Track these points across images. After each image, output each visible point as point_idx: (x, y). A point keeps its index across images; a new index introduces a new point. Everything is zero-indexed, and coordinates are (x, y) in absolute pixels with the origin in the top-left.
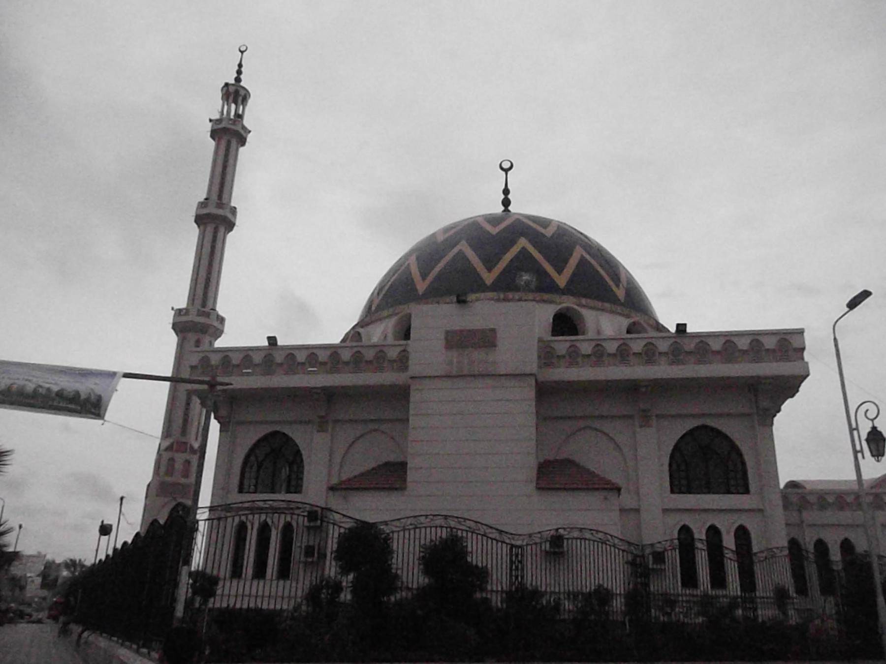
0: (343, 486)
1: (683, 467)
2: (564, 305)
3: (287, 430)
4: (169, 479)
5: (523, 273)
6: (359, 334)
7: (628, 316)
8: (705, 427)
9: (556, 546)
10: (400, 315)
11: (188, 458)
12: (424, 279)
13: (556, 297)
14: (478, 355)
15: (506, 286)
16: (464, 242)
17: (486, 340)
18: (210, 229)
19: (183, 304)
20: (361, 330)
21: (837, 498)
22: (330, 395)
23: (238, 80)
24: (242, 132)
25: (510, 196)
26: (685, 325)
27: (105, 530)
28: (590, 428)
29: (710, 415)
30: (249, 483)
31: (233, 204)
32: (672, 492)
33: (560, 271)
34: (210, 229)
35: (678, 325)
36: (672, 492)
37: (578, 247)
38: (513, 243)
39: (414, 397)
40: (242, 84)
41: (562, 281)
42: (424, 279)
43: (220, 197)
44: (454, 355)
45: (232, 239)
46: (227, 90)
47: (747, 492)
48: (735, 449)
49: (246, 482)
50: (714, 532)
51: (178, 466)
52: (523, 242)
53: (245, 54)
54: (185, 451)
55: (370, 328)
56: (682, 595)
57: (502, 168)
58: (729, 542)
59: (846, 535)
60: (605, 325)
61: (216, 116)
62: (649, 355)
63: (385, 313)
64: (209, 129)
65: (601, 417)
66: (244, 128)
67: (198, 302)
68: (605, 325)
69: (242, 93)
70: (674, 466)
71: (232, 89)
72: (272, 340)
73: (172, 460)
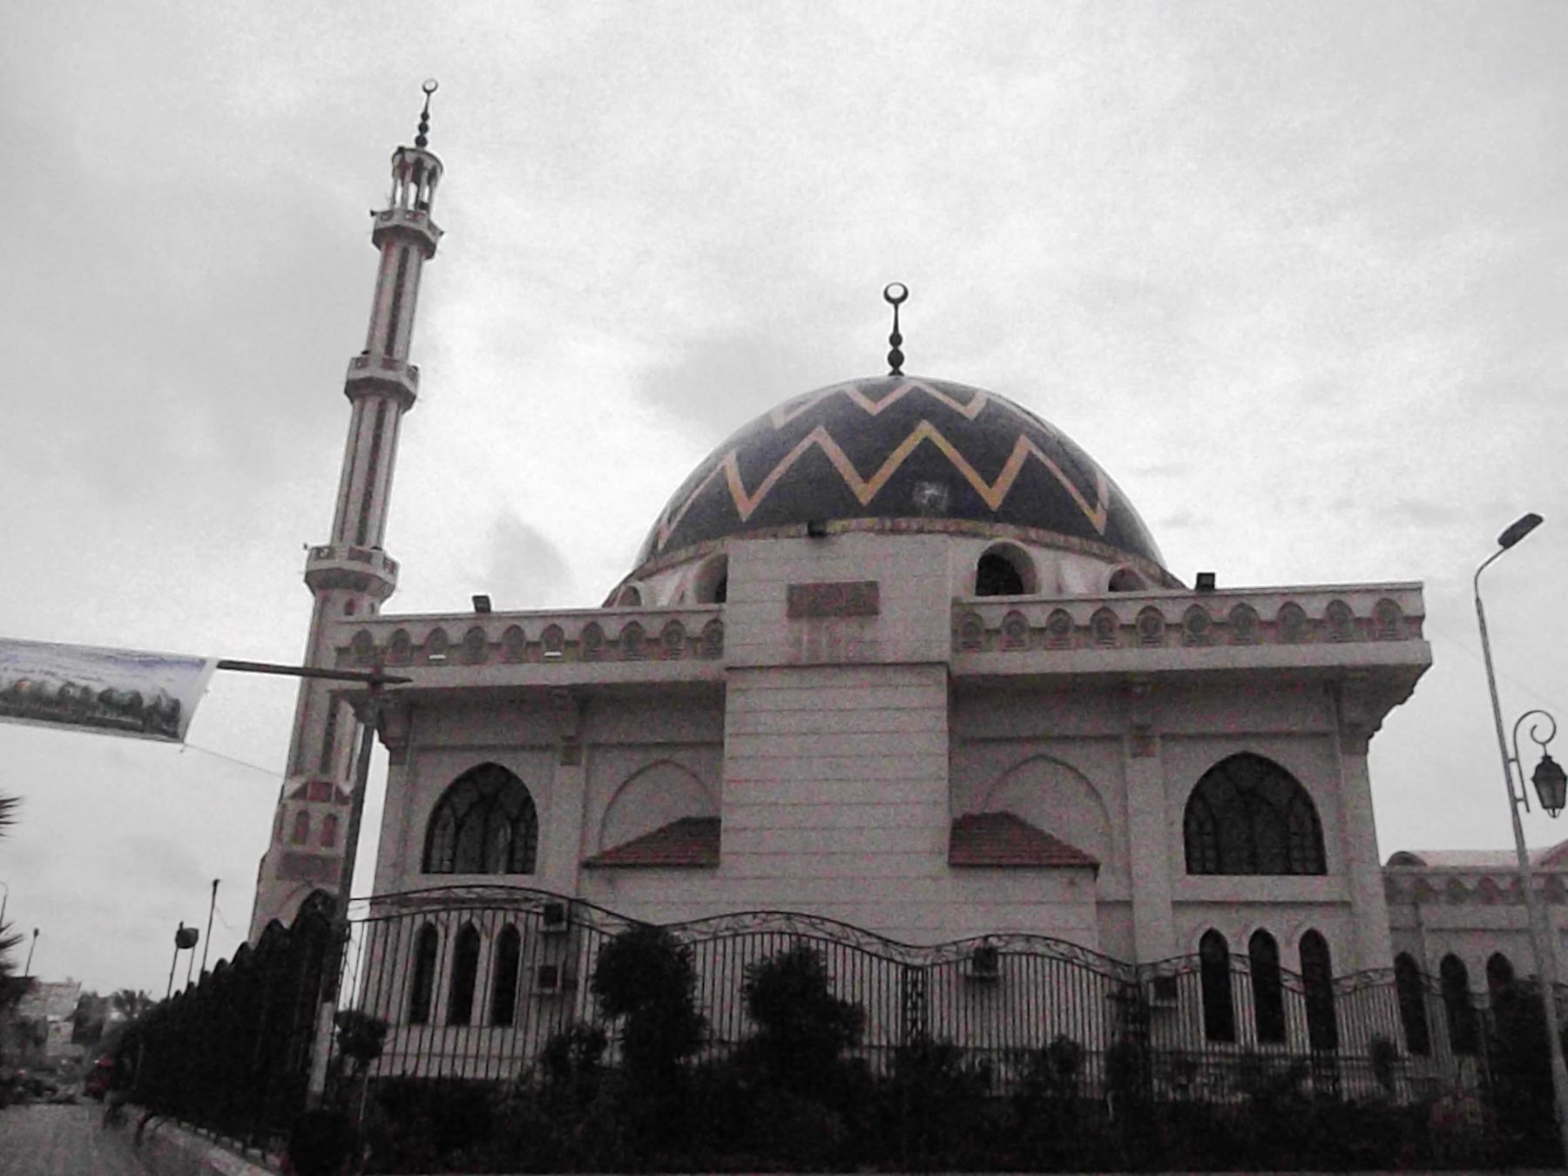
1: (1209, 828)
2: (999, 540)
3: (507, 762)
4: (298, 848)
5: (926, 484)
6: (635, 591)
7: (1111, 560)
8: (1247, 756)
9: (984, 968)
10: (707, 558)
11: (333, 811)
12: (750, 494)
13: (985, 528)
14: (846, 629)
15: (896, 506)
16: (821, 429)
17: (860, 601)
18: (371, 406)
19: (323, 538)
20: (639, 585)
21: (1481, 883)
22: (584, 699)
23: (421, 141)
24: (429, 234)
25: (902, 348)
26: (1212, 575)
27: (186, 939)
28: (1043, 757)
29: (1257, 736)
30: (440, 855)
31: (412, 362)
32: (1190, 871)
33: (990, 481)
34: (371, 406)
35: (1200, 576)
36: (1190, 871)
37: (1023, 438)
38: (908, 429)
39: (733, 703)
40: (428, 148)
41: (994, 497)
42: (750, 494)
43: (389, 348)
44: (804, 627)
46: (403, 160)
47: (1321, 870)
48: (1300, 795)
49: (436, 855)
50: (1263, 942)
51: (316, 825)
52: (925, 429)
53: (433, 95)
54: (328, 799)
55: (656, 581)
56: (1207, 1055)
57: (888, 298)
58: (1290, 959)
60: (1069, 574)
61: (383, 206)
62: (1149, 628)
63: (682, 554)
64: (371, 229)
65: (1065, 739)
66: (431, 226)
68: (1069, 574)
69: (429, 164)
70: (1194, 826)
71: (410, 158)
72: (482, 603)
73: (304, 815)
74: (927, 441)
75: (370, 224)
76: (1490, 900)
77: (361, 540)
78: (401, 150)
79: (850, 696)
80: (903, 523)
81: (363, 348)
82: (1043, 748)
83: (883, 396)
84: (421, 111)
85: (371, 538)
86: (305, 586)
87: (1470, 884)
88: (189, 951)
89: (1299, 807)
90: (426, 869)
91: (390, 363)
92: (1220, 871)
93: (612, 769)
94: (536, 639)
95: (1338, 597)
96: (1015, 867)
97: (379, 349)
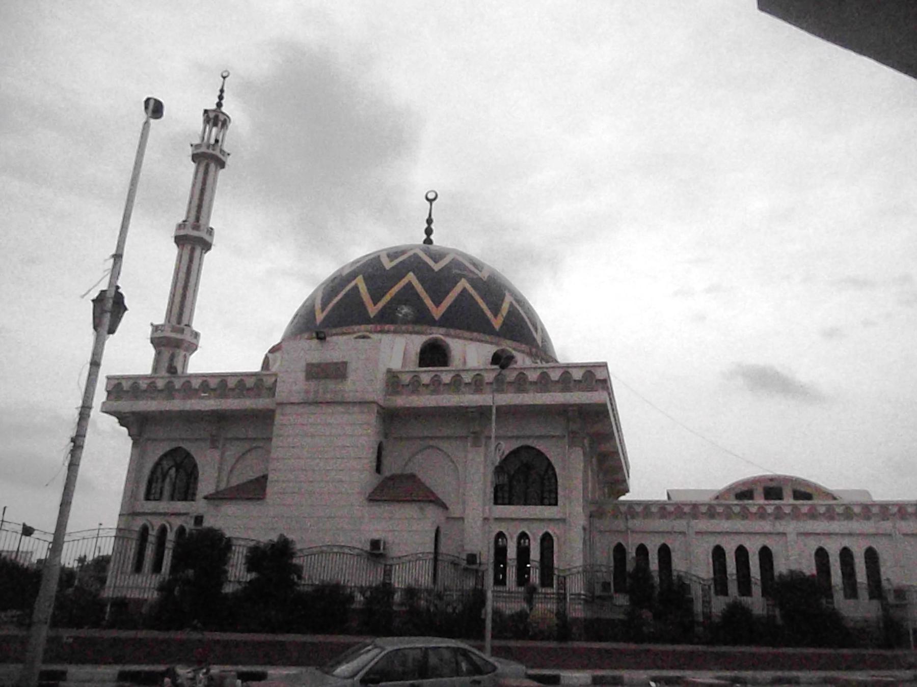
0: (220, 496)
2: (434, 336)
5: (403, 306)
7: (497, 344)
8: (528, 448)
9: (376, 551)
14: (331, 385)
15: (387, 319)
16: (360, 277)
19: (160, 320)
21: (759, 509)
22: (220, 418)
23: (219, 105)
24: (221, 156)
28: (432, 447)
31: (211, 225)
33: (438, 303)
39: (278, 418)
43: (198, 219)
44: (313, 384)
45: (210, 259)
46: (208, 116)
52: (411, 277)
53: (227, 79)
57: (427, 199)
59: (717, 543)
60: (471, 353)
61: (197, 141)
64: (190, 153)
65: (442, 438)
66: (222, 151)
67: (174, 320)
68: (471, 353)
69: (222, 118)
71: (212, 115)
74: (409, 285)
75: (190, 151)
76: (868, 518)
77: (179, 323)
78: (206, 111)
79: (337, 418)
80: (386, 327)
81: (184, 219)
82: (431, 443)
83: (396, 257)
84: (219, 88)
85: (185, 321)
86: (151, 345)
87: (857, 510)
88: (28, 538)
89: (550, 472)
90: (147, 498)
91: (196, 227)
92: (510, 504)
93: (233, 451)
94: (197, 387)
95: (589, 369)
96: (404, 501)
97: (192, 219)
